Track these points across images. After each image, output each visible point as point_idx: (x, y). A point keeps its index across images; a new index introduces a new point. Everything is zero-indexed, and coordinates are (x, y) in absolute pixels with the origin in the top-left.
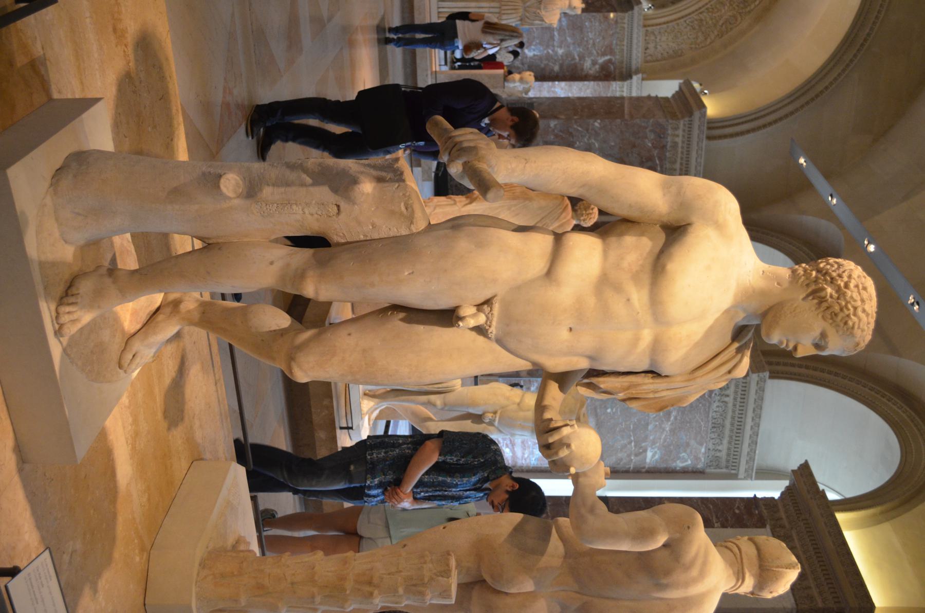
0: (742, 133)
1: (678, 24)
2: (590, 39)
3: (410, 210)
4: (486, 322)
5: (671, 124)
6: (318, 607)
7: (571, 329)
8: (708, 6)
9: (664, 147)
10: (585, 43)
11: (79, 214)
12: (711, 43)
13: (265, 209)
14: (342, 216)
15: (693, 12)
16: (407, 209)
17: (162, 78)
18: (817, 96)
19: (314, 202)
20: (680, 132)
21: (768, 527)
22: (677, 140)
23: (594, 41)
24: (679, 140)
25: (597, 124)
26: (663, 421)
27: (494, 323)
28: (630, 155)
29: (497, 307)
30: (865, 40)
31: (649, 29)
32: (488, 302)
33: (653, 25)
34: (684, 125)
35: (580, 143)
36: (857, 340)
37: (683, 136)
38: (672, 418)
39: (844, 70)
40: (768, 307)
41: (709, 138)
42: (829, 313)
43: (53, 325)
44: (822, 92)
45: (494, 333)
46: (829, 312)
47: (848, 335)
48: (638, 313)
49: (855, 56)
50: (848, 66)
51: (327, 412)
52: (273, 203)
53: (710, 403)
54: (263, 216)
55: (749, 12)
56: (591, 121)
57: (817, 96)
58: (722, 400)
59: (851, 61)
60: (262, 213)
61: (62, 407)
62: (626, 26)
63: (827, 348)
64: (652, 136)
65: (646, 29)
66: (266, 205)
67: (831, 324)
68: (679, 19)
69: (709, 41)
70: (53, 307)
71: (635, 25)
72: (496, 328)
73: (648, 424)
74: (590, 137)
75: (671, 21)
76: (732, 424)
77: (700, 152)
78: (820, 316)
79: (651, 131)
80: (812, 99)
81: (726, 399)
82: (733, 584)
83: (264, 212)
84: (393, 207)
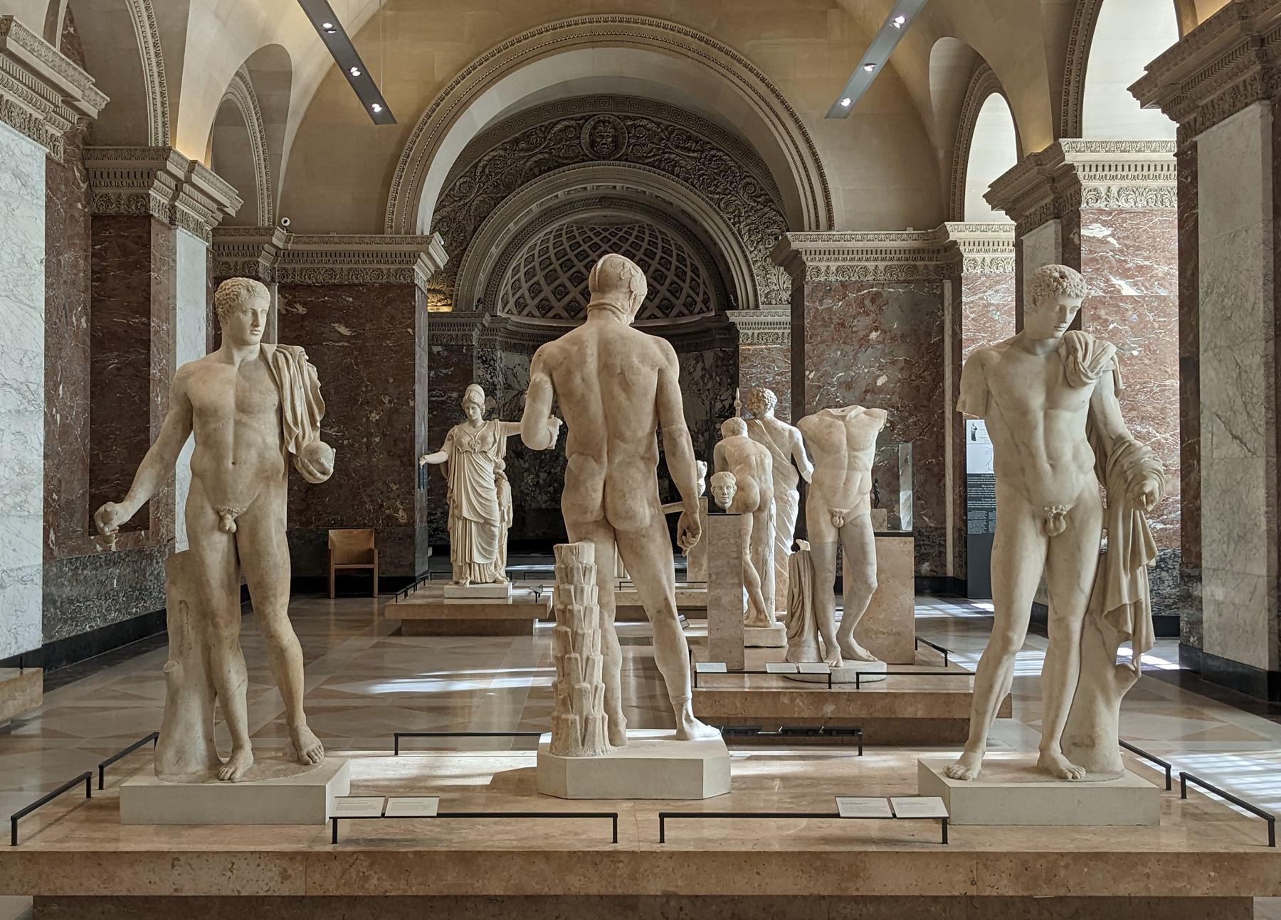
0: (824, 183)
1: (755, 262)
2: (774, 379)
5: (811, 278)
6: (585, 657)
8: (730, 223)
9: (843, 284)
10: (780, 386)
12: (781, 215)
15: (738, 242)
18: (773, 91)
20: (823, 265)
21: (1195, 139)
22: (833, 269)
23: (778, 375)
24: (834, 266)
25: (811, 376)
26: (1152, 277)
28: (854, 329)
30: (701, 39)
31: (761, 299)
33: (756, 295)
34: (812, 260)
35: (837, 397)
37: (828, 260)
38: (1147, 263)
39: (739, 61)
41: (830, 226)
44: (768, 85)
49: (720, 49)
50: (734, 57)
51: (797, 701)
53: (1121, 212)
55: (739, 167)
56: (807, 382)
57: (773, 91)
58: (1116, 195)
59: (727, 53)
62: (756, 332)
64: (828, 302)
65: (761, 306)
68: (747, 261)
69: (778, 218)
70: (217, 781)
71: (755, 319)
73: (1158, 297)
74: (829, 384)
75: (750, 271)
76: (1157, 178)
77: (859, 237)
79: (821, 304)
80: (778, 96)
81: (1114, 190)
82: (610, 312)
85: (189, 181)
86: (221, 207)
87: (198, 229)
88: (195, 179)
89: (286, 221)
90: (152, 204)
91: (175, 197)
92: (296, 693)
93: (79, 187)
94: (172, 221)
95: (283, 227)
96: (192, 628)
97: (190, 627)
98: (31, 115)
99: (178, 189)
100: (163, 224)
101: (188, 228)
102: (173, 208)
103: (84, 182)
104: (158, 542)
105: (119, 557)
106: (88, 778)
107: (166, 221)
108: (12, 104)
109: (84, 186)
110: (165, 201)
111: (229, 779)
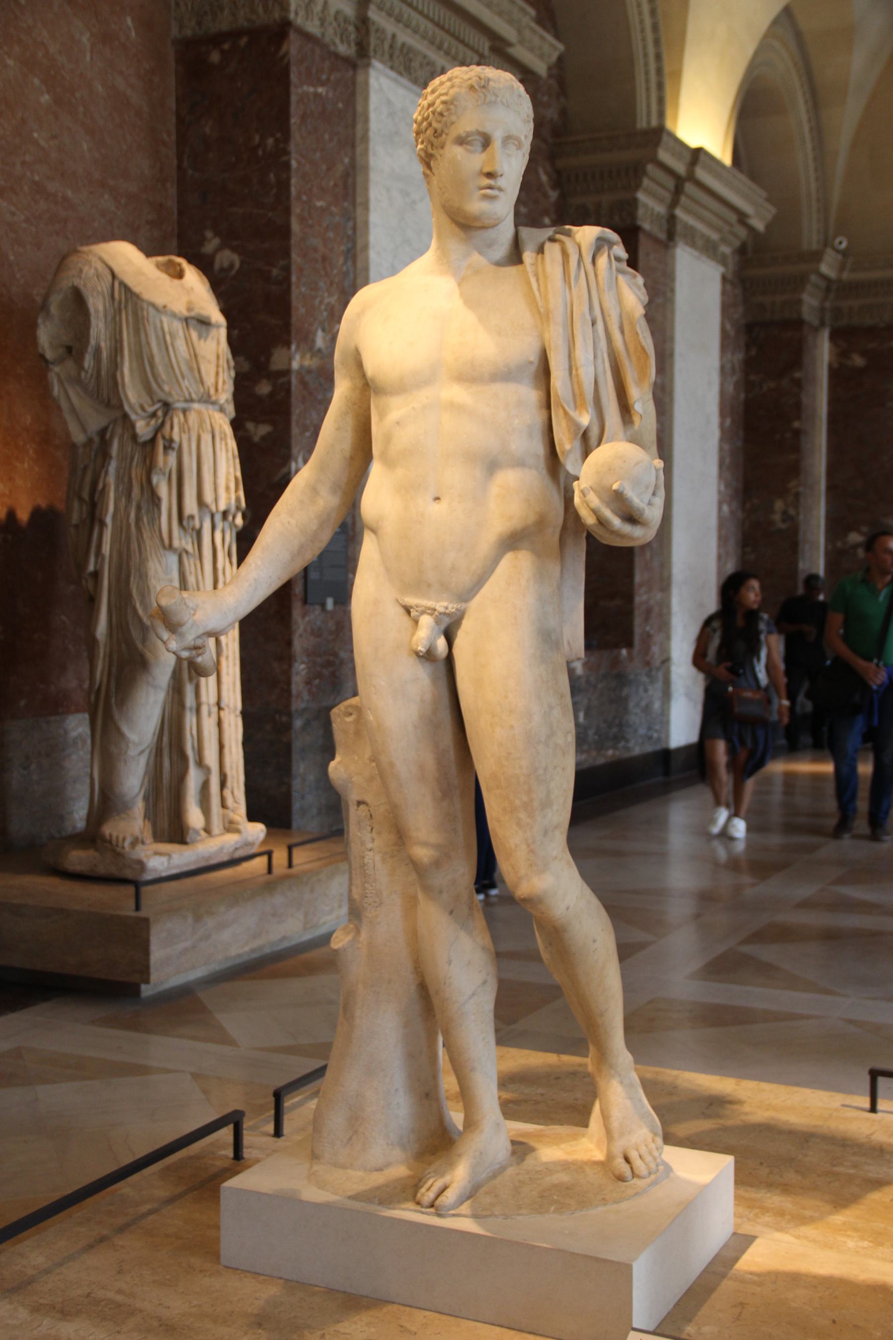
3: (350, 710)
4: (429, 614)
7: (437, 499)
11: (350, 1138)
13: (371, 899)
14: (368, 798)
16: (351, 714)
17: (443, 1042)
19: (359, 834)
27: (430, 603)
29: (410, 600)
32: (408, 610)
36: (463, 91)
40: (453, 225)
42: (436, 140)
43: (427, 1213)
45: (446, 604)
46: (435, 141)
47: (456, 106)
48: (413, 408)
52: (365, 887)
54: (381, 904)
60: (376, 904)
61: (534, 1247)
63: (477, 130)
66: (366, 897)
67: (447, 134)
70: (411, 1205)
72: (437, 601)
78: (441, 152)
83: (376, 902)
84: (351, 731)
85: (691, 177)
86: (742, 218)
87: (709, 249)
88: (701, 174)
89: (840, 243)
90: (641, 212)
91: (674, 203)
92: (602, 1015)
93: (545, 195)
94: (671, 235)
95: (834, 249)
96: (384, 860)
97: (378, 858)
98: (394, 36)
99: (678, 191)
100: (656, 240)
101: (693, 245)
102: (672, 219)
103: (554, 188)
104: (648, 664)
105: (588, 682)
106: (235, 1120)
107: (663, 236)
108: (410, 50)
109: (553, 195)
110: (660, 209)
111: (432, 1206)
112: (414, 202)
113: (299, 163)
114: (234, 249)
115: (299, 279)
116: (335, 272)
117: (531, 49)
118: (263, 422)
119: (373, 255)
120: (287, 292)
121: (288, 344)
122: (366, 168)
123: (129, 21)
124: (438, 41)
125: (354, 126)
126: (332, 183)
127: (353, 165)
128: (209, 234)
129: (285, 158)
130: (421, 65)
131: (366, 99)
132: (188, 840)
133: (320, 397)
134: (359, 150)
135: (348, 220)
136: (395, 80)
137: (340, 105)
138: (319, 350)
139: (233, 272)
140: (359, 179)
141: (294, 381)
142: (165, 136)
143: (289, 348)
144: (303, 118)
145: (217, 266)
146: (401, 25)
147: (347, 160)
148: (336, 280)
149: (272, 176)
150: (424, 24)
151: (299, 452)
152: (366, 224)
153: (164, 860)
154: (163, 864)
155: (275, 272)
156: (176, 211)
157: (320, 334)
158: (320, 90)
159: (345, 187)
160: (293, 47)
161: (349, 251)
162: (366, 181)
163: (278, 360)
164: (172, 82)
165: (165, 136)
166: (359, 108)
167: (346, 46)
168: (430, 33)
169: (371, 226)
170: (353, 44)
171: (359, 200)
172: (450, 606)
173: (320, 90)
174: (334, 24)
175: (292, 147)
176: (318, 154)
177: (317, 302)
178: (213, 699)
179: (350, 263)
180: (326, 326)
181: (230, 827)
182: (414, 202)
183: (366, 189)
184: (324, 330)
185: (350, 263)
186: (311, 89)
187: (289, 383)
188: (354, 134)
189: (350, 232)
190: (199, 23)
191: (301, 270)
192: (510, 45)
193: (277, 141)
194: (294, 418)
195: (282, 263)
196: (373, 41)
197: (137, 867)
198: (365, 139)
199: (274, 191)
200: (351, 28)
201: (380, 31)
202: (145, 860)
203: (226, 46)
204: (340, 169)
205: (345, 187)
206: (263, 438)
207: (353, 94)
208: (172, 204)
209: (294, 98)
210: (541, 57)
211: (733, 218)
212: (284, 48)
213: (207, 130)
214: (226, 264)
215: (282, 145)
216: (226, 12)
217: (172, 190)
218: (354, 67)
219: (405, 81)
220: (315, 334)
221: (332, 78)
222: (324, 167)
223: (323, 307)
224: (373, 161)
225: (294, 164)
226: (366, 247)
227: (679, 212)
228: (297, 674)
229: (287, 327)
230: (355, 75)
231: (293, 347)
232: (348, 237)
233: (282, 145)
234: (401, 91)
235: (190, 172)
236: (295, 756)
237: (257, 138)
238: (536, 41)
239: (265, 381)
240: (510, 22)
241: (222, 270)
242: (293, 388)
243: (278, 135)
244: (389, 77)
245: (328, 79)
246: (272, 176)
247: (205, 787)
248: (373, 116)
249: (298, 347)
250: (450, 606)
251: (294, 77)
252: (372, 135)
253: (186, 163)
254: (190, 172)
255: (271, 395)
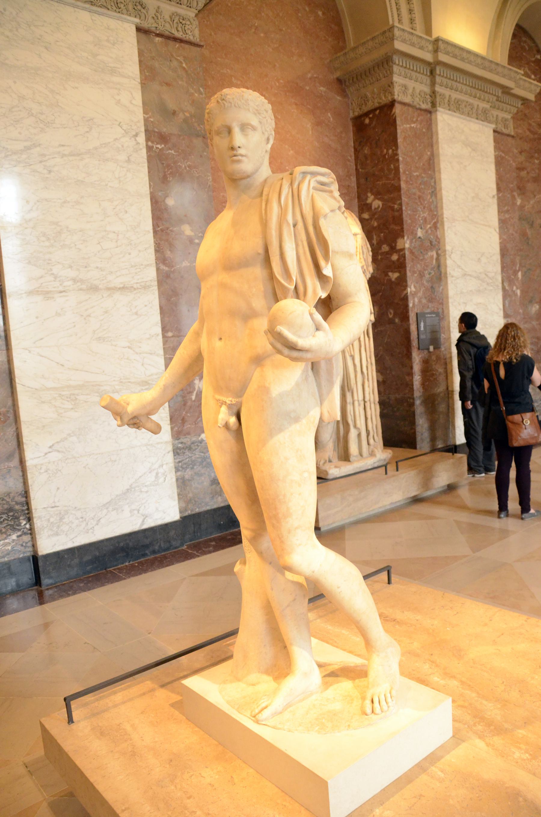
91: (433, 84)
112: (465, 166)
113: (403, 158)
114: (379, 199)
115: (406, 208)
116: (426, 202)
117: (525, 89)
118: (395, 272)
119: (444, 192)
120: (401, 215)
121: (403, 237)
122: (438, 155)
123: (329, 115)
124: (473, 94)
125: (432, 138)
126: (422, 164)
127: (432, 154)
128: (369, 195)
129: (396, 157)
130: (466, 106)
131: (437, 125)
132: (351, 460)
133: (421, 258)
134: (435, 148)
135: (432, 179)
136: (451, 115)
137: (424, 130)
138: (419, 238)
139: (380, 209)
140: (436, 161)
141: (407, 253)
142: (349, 158)
143: (404, 238)
144: (405, 138)
145: (373, 208)
146: (453, 91)
147: (429, 153)
148: (427, 206)
149: (392, 165)
150: (464, 88)
151: (411, 283)
152: (440, 179)
153: (337, 470)
154: (337, 471)
155: (396, 206)
156: (356, 187)
157: (419, 230)
158: (413, 125)
159: (429, 164)
160: (398, 110)
161: (432, 192)
162: (439, 160)
163: (400, 244)
164: (351, 135)
165: (349, 158)
166: (434, 130)
167: (425, 104)
168: (469, 91)
169: (442, 180)
170: (429, 103)
171: (436, 169)
172: (233, 400)
173: (413, 125)
174: (418, 96)
175: (399, 152)
176: (413, 153)
177: (417, 217)
178: (361, 397)
179: (433, 198)
180: (422, 227)
181: (372, 454)
182: (465, 166)
183: (439, 164)
184: (421, 228)
185: (433, 198)
186: (408, 126)
187: (405, 254)
188: (432, 141)
189: (433, 184)
190: (360, 109)
191: (408, 204)
192: (512, 89)
193: (393, 150)
194: (408, 269)
195: (398, 202)
196: (438, 99)
197: (325, 473)
198: (437, 142)
199: (393, 172)
200: (428, 97)
201: (442, 96)
202: (328, 470)
203: (371, 116)
204: (426, 157)
205: (429, 164)
206: (396, 279)
207: (430, 125)
208: (354, 184)
209: (399, 131)
210: (531, 91)
211: (499, 92)
212: (394, 111)
213: (366, 152)
214: (377, 206)
215: (395, 152)
216: (370, 101)
217: (354, 179)
218: (430, 112)
219: (457, 114)
220: (417, 231)
221: (419, 119)
222: (417, 158)
223: (420, 219)
224: (441, 151)
225: (401, 159)
226: (441, 189)
227: (438, 88)
228: (416, 381)
229: (402, 229)
230: (431, 116)
231: (406, 238)
232: (432, 186)
233: (395, 152)
234: (455, 119)
235: (360, 170)
236: (417, 417)
237: (385, 151)
238: (527, 85)
239: (395, 254)
240: (510, 79)
241: (375, 209)
242: (407, 256)
243: (394, 148)
244: (447, 114)
245: (417, 120)
246: (392, 165)
247: (359, 435)
248: (440, 132)
249: (408, 237)
250: (233, 400)
251: (398, 122)
252: (440, 140)
253: (359, 167)
254: (360, 170)
255: (398, 259)
